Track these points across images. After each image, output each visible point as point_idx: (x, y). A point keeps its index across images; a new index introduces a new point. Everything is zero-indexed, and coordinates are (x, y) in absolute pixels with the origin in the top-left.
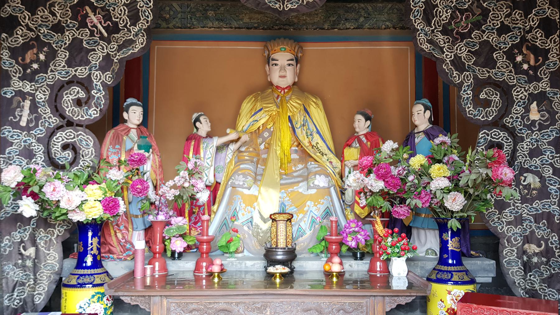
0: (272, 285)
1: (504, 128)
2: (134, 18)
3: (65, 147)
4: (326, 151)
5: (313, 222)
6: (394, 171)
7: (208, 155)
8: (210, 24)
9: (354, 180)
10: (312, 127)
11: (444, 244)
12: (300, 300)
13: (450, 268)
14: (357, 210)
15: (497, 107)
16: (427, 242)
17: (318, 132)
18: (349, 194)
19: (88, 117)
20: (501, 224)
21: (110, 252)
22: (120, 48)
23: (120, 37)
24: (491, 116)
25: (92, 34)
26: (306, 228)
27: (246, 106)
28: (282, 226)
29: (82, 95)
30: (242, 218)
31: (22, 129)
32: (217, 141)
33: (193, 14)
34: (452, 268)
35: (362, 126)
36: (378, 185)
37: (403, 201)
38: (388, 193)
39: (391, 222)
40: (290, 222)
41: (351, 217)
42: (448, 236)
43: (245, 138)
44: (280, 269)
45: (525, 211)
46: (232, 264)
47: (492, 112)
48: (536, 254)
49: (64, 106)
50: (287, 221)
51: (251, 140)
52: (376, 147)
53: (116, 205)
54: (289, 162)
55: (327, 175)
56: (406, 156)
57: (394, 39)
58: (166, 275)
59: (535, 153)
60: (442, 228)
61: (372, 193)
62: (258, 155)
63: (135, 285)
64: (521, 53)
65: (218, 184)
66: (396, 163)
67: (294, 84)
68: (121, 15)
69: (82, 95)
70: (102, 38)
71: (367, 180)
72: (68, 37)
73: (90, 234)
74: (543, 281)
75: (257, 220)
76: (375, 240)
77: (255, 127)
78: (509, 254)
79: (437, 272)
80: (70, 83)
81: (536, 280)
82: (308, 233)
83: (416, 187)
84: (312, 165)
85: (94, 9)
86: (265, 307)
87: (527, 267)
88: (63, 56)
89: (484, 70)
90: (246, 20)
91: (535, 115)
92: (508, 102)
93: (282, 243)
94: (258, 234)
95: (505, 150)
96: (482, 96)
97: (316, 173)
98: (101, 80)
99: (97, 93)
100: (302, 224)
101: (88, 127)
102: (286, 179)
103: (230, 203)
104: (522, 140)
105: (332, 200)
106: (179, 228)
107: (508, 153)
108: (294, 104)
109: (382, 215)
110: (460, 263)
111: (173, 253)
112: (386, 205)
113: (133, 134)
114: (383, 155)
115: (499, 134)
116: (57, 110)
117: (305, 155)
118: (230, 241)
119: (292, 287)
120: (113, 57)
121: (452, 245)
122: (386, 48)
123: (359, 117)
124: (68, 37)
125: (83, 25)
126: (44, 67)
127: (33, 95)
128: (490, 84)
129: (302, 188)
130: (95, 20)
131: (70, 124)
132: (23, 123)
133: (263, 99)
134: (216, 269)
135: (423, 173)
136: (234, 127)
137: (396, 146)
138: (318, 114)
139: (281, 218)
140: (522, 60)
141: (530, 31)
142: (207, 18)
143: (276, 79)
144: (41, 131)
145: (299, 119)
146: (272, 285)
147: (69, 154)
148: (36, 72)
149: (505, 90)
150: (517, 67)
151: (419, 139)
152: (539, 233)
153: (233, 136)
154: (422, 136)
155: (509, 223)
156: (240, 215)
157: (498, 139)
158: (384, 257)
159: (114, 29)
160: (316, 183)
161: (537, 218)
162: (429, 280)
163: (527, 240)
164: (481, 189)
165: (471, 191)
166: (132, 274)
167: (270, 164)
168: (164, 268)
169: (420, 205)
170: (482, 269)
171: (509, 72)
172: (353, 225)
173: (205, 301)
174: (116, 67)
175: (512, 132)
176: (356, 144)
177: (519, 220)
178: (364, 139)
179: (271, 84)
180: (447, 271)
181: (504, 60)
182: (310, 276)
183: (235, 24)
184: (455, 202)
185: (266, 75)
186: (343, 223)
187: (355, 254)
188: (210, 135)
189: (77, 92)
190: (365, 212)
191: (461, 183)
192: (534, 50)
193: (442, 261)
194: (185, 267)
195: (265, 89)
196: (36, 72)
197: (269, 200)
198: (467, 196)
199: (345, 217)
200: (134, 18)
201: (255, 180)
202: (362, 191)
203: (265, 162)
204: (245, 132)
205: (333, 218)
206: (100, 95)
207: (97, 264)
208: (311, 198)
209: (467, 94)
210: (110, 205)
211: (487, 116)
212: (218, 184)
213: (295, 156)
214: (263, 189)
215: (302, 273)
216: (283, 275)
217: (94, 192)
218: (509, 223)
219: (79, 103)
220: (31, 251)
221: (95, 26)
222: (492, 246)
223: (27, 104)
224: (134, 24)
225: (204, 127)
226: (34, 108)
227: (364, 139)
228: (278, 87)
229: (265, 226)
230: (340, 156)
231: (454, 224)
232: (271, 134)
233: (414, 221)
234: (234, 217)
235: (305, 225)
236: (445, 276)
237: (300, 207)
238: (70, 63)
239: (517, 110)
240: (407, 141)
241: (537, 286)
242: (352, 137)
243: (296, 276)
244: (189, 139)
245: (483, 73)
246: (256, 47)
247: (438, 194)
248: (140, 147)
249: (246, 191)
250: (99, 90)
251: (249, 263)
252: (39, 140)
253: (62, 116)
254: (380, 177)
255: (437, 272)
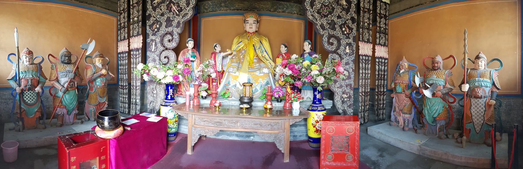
0: (242, 112)
1: (338, 54)
2: (188, 4)
3: (165, 57)
4: (269, 59)
5: (261, 87)
6: (296, 67)
7: (219, 60)
8: (223, 9)
9: (279, 70)
10: (263, 48)
11: (315, 96)
12: (253, 120)
13: (317, 105)
14: (280, 82)
16: (308, 95)
17: (266, 51)
18: (277, 76)
20: (335, 88)
21: (181, 94)
22: (183, 17)
23: (183, 13)
25: (173, 14)
26: (258, 89)
27: (235, 41)
28: (248, 88)
29: (170, 38)
30: (232, 84)
31: (153, 52)
32: (223, 54)
33: (216, 5)
35: (283, 50)
36: (290, 72)
37: (299, 79)
38: (293, 76)
39: (294, 88)
41: (277, 85)
42: (316, 93)
43: (234, 53)
44: (246, 106)
45: (343, 83)
46: (225, 102)
47: (334, 48)
48: (346, 98)
49: (165, 42)
51: (237, 54)
52: (289, 58)
53: (178, 78)
54: (253, 63)
55: (268, 68)
56: (301, 61)
57: (298, 18)
58: (199, 105)
59: (347, 64)
60: (315, 90)
61: (286, 76)
62: (240, 60)
63: (186, 109)
64: (344, 27)
65: (224, 71)
66: (297, 64)
67: (256, 31)
68: (183, 3)
69: (170, 38)
70: (177, 15)
71: (284, 70)
72: (166, 16)
73: (170, 88)
74: (348, 106)
75: (238, 85)
76: (287, 95)
77: (239, 49)
78: (337, 98)
80: (166, 34)
81: (346, 106)
82: (259, 91)
83: (304, 73)
84: (262, 64)
85: (174, 4)
86: (237, 122)
87: (343, 102)
88: (164, 24)
90: (237, 6)
91: (348, 51)
92: (339, 45)
93: (248, 95)
94: (238, 91)
96: (331, 41)
97: (264, 67)
98: (177, 31)
100: (257, 87)
101: (172, 50)
102: (251, 69)
103: (227, 78)
104: (343, 59)
105: (270, 78)
106: (204, 87)
108: (256, 40)
109: (290, 85)
110: (321, 103)
111: (202, 97)
112: (292, 81)
113: (190, 52)
114: (292, 60)
116: (162, 45)
117: (260, 60)
118: (225, 93)
119: (250, 114)
121: (318, 96)
122: (296, 21)
123: (282, 46)
124: (166, 16)
125: (170, 11)
126: (159, 29)
127: (155, 40)
129: (257, 73)
130: (174, 8)
131: (167, 49)
132: (153, 50)
133: (243, 37)
134: (217, 105)
135: (308, 68)
136: (230, 48)
137: (297, 56)
138: (266, 44)
141: (347, 20)
142: (221, 6)
143: (248, 29)
144: (158, 52)
145: (257, 46)
146: (242, 112)
147: (166, 60)
148: (156, 32)
149: (339, 40)
150: (343, 32)
151: (306, 56)
152: (347, 91)
153: (229, 52)
154: (307, 54)
155: (338, 88)
156: (231, 83)
158: (290, 101)
159: (180, 10)
160: (264, 71)
161: (347, 86)
162: (308, 110)
163: (343, 93)
164: (331, 75)
165: (327, 76)
166: (185, 103)
167: (244, 63)
168: (199, 102)
169: (307, 81)
170: (327, 104)
172: (278, 89)
173: (210, 118)
174: (181, 25)
175: (340, 56)
176: (281, 57)
177: (341, 87)
178: (284, 55)
179: (246, 31)
182: (259, 108)
183: (232, 8)
184: (321, 80)
185: (244, 28)
186: (274, 87)
187: (279, 100)
188: (220, 52)
189: (169, 37)
190: (284, 83)
191: (323, 73)
192: (348, 27)
193: (314, 103)
194: (206, 102)
195: (244, 34)
196: (156, 32)
197: (243, 77)
198: (325, 77)
199: (275, 85)
200: (188, 4)
201: (238, 70)
202: (282, 75)
203: (242, 62)
204: (235, 51)
205: (269, 86)
206: (176, 37)
207: (172, 99)
208: (261, 77)
209: (325, 39)
210: (176, 78)
212: (224, 71)
213: (255, 61)
214: (241, 73)
215: (255, 107)
216: (247, 108)
217: (170, 73)
218: (338, 88)
219: (169, 41)
220: (155, 92)
221: (174, 11)
222: (331, 95)
223: (154, 43)
224: (188, 7)
225: (218, 49)
226: (156, 45)
227: (284, 55)
228: (249, 32)
229: (241, 88)
230: (274, 61)
231: (319, 88)
232: (245, 52)
233: (302, 87)
234: (229, 84)
235: (258, 88)
236: (315, 108)
237: (256, 81)
238: (166, 27)
239: (342, 47)
240: (302, 55)
241: (346, 108)
242: (280, 54)
243: (253, 108)
244: (212, 54)
245: (332, 32)
246: (240, 17)
247: (315, 77)
248: (191, 57)
249: (233, 74)
251: (233, 102)
252: (157, 56)
253: (164, 47)
254: (290, 69)
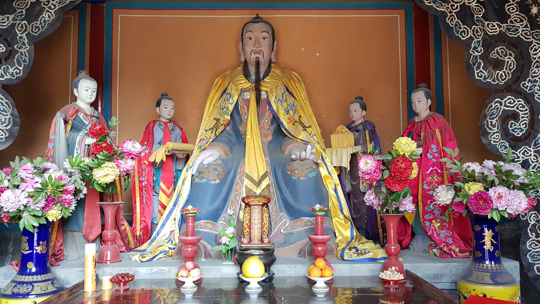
1: (519, 93)
15: (510, 70)
19: (9, 77)
24: (503, 80)
34: (35, 278)
40: (267, 207)
47: (503, 76)
50: (263, 205)
79: (14, 284)
89: (494, 24)
95: (521, 120)
96: (493, 55)
99: (21, 48)
107: (525, 123)
115: (514, 101)
120: (44, 4)
128: (504, 41)
139: (257, 203)
140: (538, 12)
157: (513, 107)
171: (525, 27)
180: (27, 283)
181: (517, 13)
211: (498, 79)
245: (494, 28)
250: (24, 44)
255: (14, 284)
